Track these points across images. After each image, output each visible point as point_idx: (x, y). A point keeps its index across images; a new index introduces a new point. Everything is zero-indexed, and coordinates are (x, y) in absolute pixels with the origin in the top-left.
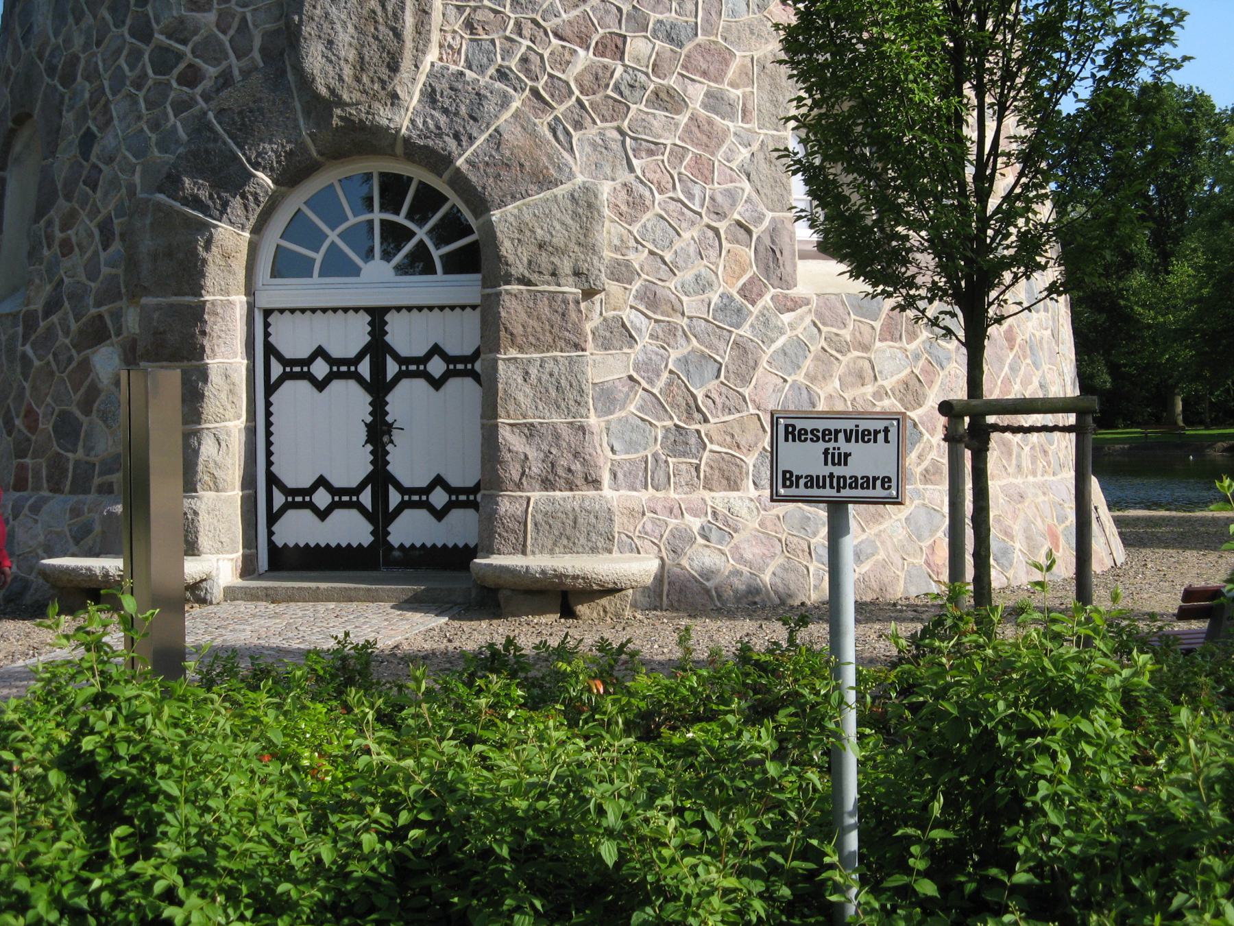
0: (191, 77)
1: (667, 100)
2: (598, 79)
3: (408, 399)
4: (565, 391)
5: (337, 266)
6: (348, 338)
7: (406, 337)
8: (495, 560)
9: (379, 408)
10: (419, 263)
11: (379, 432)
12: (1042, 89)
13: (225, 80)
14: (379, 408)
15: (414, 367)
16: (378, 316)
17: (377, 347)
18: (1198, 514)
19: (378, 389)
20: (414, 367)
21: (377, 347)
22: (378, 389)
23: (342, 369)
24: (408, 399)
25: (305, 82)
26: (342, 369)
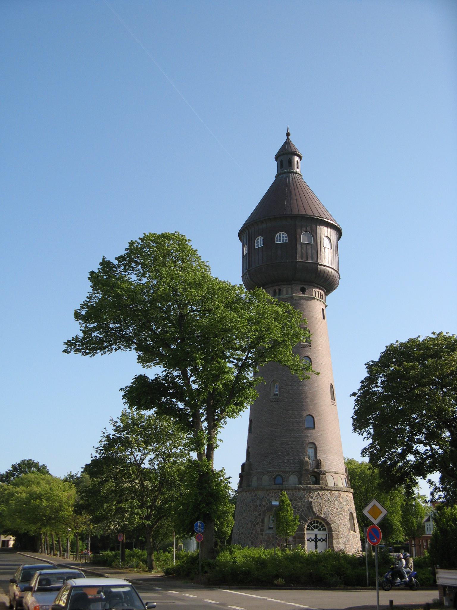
0: (299, 510)
1: (342, 514)
2: (336, 512)
3: (319, 543)
4: (338, 543)
5: (312, 530)
6: (313, 537)
7: (319, 537)
8: (52, 586)
9: (316, 544)
10: (320, 530)
11: (316, 547)
12: (178, 344)
13: (303, 511)
14: (316, 544)
15: (319, 540)
16: (316, 535)
17: (316, 538)
18: (367, 562)
19: (316, 542)
20: (319, 540)
21: (316, 538)
22: (316, 542)
23: (313, 540)
24: (319, 543)
25: (313, 512)
26: (313, 540)
